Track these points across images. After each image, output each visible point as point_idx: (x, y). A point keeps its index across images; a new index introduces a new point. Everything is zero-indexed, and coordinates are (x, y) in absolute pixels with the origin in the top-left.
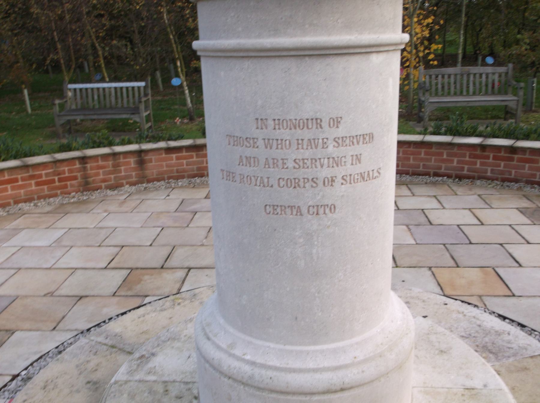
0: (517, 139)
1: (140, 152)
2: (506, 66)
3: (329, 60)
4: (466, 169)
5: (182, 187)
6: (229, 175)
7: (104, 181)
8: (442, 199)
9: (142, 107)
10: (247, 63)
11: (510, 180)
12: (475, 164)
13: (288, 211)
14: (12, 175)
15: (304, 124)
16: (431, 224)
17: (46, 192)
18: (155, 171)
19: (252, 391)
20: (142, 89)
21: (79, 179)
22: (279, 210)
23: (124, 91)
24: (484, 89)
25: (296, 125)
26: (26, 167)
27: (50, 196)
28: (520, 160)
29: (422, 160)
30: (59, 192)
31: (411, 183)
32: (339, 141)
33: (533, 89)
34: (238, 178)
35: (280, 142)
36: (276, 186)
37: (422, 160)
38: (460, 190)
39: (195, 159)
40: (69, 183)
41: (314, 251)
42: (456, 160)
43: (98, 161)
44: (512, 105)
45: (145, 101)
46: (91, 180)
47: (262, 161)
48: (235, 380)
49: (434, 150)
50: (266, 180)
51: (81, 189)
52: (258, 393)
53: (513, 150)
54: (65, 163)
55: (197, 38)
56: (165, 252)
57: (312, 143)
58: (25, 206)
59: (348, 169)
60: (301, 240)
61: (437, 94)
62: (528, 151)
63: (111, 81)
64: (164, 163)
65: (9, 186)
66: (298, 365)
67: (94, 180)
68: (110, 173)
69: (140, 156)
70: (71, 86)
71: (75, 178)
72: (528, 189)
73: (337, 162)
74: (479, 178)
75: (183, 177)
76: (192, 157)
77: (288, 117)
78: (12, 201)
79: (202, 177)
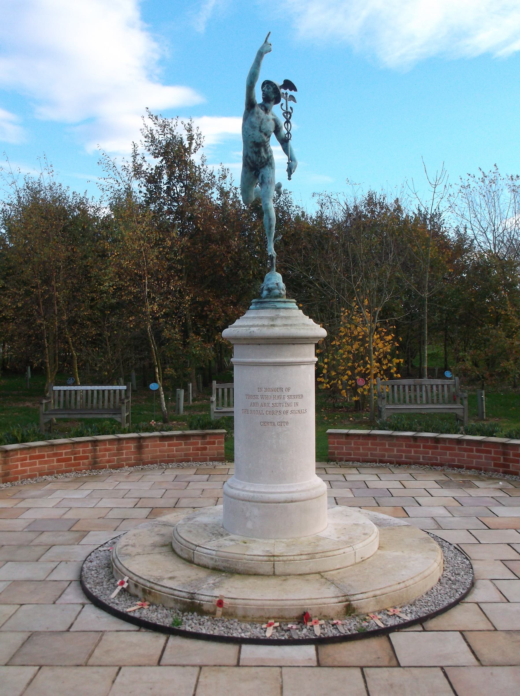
0: (442, 433)
1: (140, 438)
3: (285, 367)
4: (404, 456)
5: (172, 468)
7: (109, 461)
9: (124, 408)
10: (255, 367)
11: (437, 465)
12: (411, 452)
13: (270, 424)
14: (41, 452)
15: (276, 390)
16: (368, 487)
17: (64, 468)
18: (149, 455)
19: (253, 503)
20: (123, 392)
21: (90, 459)
23: (106, 393)
24: (435, 398)
25: (273, 390)
26: (53, 445)
27: (67, 472)
28: (443, 448)
29: (369, 449)
30: (73, 468)
31: (361, 467)
32: (290, 397)
33: (482, 400)
34: (250, 412)
35: (267, 397)
36: (265, 414)
37: (369, 449)
38: (396, 471)
39: (183, 446)
40: (81, 461)
41: (280, 441)
42: (395, 449)
43: (106, 445)
44: (460, 413)
45: (127, 403)
46: (98, 460)
47: (260, 404)
48: (246, 500)
49: (378, 441)
51: (90, 467)
52: (256, 504)
53: (436, 440)
54: (81, 445)
55: (232, 357)
56: (175, 501)
57: (279, 397)
58: (49, 478)
59: (293, 408)
60: (275, 436)
61: (393, 403)
62: (447, 441)
63: (82, 384)
64: (158, 449)
65: (37, 461)
66: (273, 491)
67: (101, 460)
68: (115, 455)
69: (139, 442)
70: (56, 388)
71: (87, 457)
72: (449, 471)
73: (289, 405)
74: (415, 463)
75: (172, 461)
76: (180, 444)
78: (37, 473)
79: (188, 462)
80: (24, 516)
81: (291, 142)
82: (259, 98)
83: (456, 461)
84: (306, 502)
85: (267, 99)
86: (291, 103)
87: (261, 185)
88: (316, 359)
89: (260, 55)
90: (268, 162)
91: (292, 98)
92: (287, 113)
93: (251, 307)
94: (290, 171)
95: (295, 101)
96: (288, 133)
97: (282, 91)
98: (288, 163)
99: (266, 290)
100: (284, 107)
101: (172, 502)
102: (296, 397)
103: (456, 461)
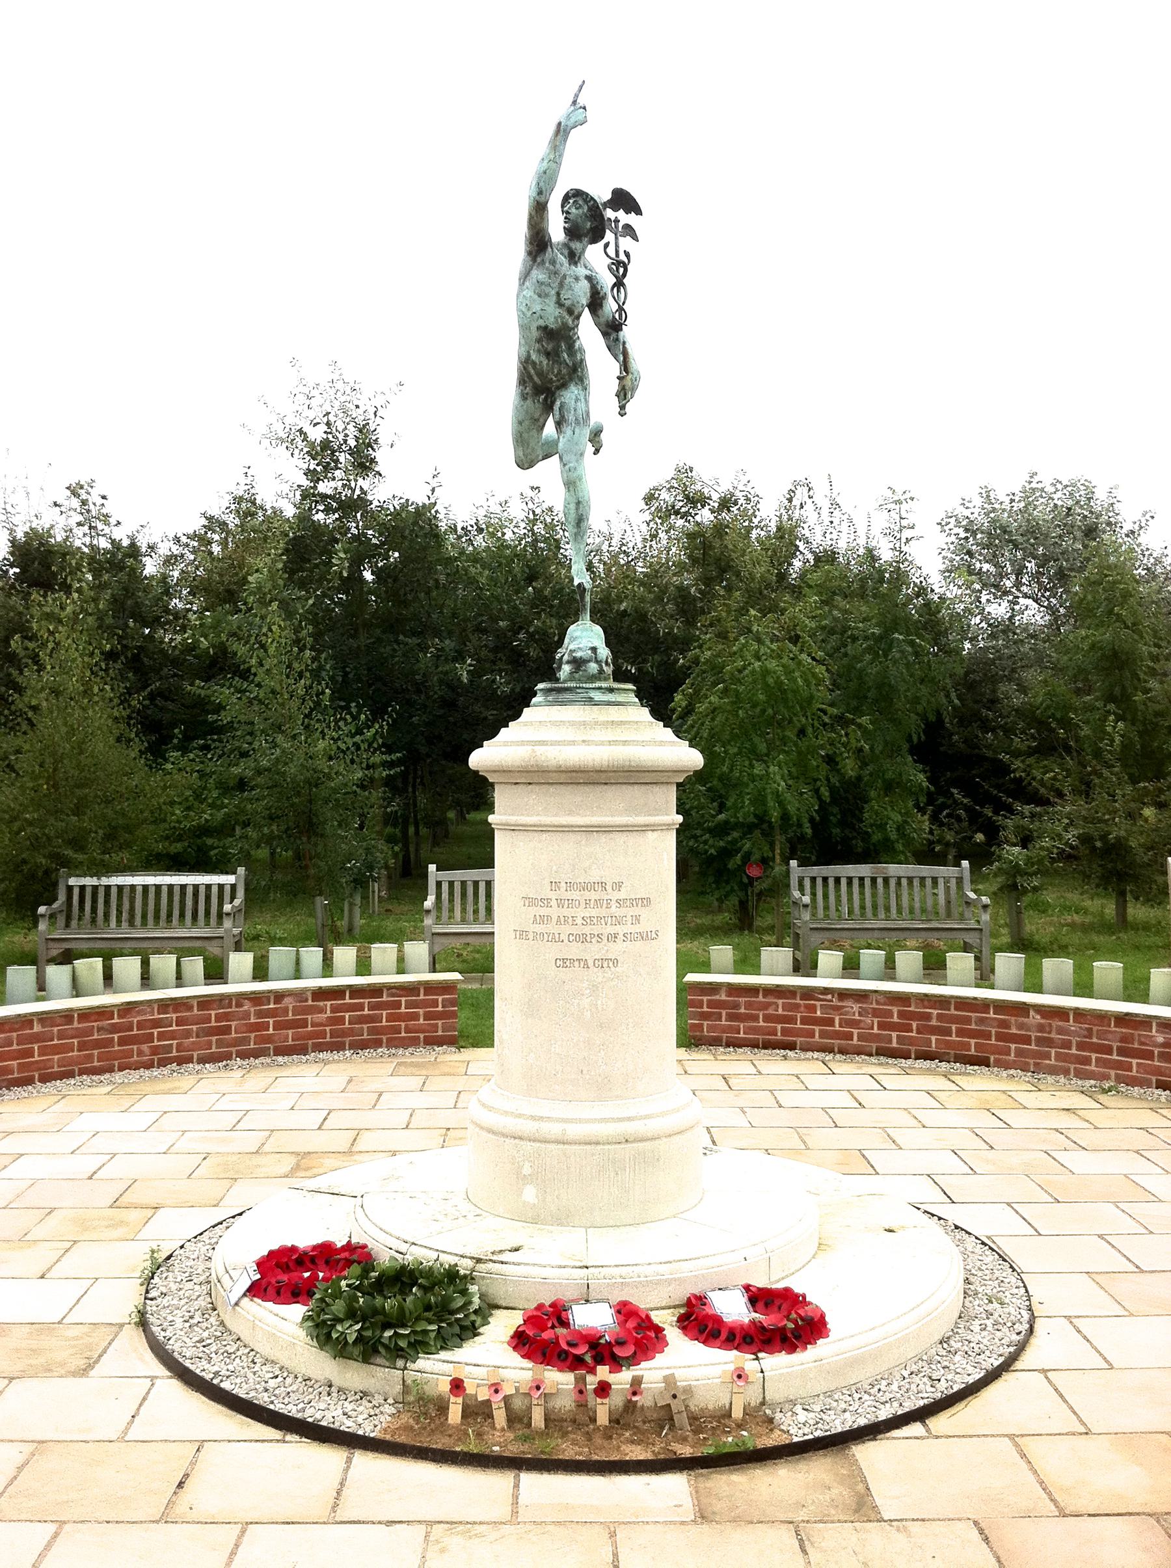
1: (297, 975)
2: (234, 873)
6: (522, 934)
8: (831, 1065)
22: (568, 963)
34: (531, 936)
36: (566, 941)
50: (557, 936)
77: (578, 881)
80: (13, 1171)
81: (627, 333)
82: (556, 230)
83: (855, 1038)
84: (657, 1142)
85: (573, 232)
86: (626, 243)
87: (559, 424)
88: (680, 819)
89: (561, 132)
90: (575, 372)
91: (629, 231)
92: (619, 263)
93: (534, 700)
94: (624, 394)
95: (635, 238)
96: (621, 309)
97: (610, 214)
98: (618, 378)
99: (568, 662)
100: (611, 251)
101: (342, 1141)
102: (634, 902)
103: (855, 1038)
